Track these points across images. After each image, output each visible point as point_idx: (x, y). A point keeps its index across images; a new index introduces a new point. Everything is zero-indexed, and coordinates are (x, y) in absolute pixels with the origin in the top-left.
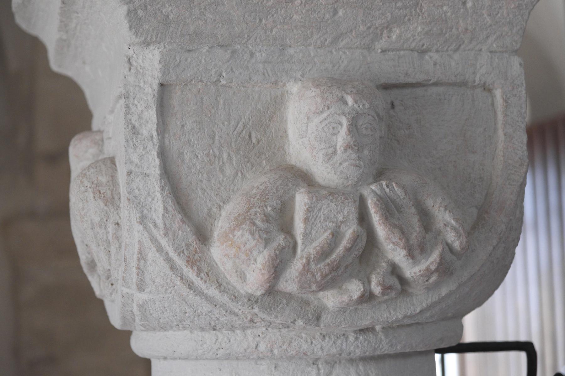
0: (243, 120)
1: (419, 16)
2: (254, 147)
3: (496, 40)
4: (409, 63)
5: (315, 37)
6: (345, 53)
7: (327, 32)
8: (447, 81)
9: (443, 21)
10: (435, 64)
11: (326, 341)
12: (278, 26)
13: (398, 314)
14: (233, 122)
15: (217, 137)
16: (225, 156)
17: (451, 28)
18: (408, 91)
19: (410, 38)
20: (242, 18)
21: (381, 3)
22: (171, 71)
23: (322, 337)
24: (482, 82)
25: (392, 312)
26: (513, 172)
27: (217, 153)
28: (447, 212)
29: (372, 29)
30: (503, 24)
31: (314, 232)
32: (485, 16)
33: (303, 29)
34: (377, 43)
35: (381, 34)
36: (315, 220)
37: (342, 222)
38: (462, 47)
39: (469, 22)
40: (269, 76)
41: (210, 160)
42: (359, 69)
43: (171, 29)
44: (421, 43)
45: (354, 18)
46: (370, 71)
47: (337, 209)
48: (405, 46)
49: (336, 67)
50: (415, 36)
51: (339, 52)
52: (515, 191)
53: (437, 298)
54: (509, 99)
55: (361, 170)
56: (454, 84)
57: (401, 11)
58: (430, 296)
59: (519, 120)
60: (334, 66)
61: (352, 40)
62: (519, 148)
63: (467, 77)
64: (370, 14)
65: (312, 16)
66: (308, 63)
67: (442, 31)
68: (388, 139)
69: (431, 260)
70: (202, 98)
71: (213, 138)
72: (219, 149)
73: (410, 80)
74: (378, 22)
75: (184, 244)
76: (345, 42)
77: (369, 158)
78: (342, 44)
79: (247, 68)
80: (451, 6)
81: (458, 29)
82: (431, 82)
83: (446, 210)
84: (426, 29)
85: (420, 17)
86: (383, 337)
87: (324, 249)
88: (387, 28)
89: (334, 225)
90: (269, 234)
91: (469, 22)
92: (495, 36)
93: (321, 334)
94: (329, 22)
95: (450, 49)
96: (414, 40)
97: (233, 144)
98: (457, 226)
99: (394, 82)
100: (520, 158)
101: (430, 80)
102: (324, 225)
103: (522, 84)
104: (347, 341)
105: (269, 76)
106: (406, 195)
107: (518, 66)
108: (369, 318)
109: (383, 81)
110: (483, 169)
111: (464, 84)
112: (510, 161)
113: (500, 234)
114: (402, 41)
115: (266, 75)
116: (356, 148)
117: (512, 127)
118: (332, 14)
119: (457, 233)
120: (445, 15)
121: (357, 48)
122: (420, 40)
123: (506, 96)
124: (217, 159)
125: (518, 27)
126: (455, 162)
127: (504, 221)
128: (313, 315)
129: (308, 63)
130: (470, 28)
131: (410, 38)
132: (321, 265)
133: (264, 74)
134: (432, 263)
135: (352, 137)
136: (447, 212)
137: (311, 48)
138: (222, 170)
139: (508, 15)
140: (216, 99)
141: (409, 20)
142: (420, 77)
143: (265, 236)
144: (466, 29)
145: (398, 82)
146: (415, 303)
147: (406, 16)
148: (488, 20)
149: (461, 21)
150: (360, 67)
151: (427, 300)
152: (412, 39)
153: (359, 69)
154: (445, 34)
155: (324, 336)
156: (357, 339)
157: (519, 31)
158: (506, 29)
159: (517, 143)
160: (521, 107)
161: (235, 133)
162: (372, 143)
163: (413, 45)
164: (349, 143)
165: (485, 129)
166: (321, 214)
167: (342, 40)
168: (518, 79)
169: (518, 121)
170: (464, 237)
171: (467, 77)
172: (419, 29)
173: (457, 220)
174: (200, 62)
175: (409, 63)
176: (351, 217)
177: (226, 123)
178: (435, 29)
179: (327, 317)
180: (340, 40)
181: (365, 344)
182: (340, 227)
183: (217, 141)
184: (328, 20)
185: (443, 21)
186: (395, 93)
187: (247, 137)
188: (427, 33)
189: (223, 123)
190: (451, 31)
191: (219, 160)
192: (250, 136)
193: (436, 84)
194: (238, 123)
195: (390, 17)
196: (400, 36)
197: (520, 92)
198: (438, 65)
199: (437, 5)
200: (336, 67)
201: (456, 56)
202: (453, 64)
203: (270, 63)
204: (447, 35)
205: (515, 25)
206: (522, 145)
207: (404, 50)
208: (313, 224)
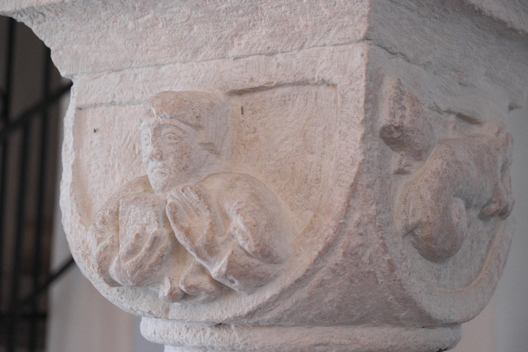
0: (131, 134)
1: (262, 20)
2: (136, 157)
3: (337, 32)
4: (255, 67)
5: (179, 54)
6: (203, 65)
7: (187, 48)
8: (287, 82)
9: (284, 21)
10: (278, 66)
11: (189, 333)
12: (151, 48)
13: (229, 313)
14: (123, 136)
15: (112, 150)
16: (117, 165)
17: (293, 27)
18: (257, 95)
19: (256, 43)
20: (124, 46)
21: (225, 14)
22: (83, 97)
23: (186, 330)
24: (320, 79)
25: (224, 311)
26: (343, 172)
27: (111, 164)
28: (239, 215)
29: (223, 39)
30: (342, 14)
31: (127, 233)
32: (323, 9)
33: (169, 48)
34: (229, 52)
35: (232, 43)
36: (127, 222)
37: (146, 225)
38: (307, 44)
39: (308, 18)
40: (146, 93)
41: (106, 170)
42: (213, 79)
43: (80, 62)
44: (266, 47)
45: (206, 32)
46: (222, 79)
47: (141, 213)
48: (253, 51)
49: (196, 80)
50: (261, 40)
51: (198, 65)
52: (344, 192)
53: (262, 301)
54: (346, 94)
55: (167, 177)
56: (295, 84)
57: (244, 18)
58: (256, 298)
59: (355, 116)
60: (194, 79)
61: (207, 52)
62: (352, 146)
63: (306, 75)
64: (218, 25)
65: (173, 35)
66: (175, 78)
67: (285, 31)
68: (237, 143)
69: (222, 262)
70: (105, 117)
71: (109, 151)
72: (113, 160)
73: (256, 85)
74: (226, 32)
75: (81, 241)
76: (202, 54)
77: (175, 165)
78: (200, 57)
79: (132, 88)
80: (287, 5)
81: (299, 27)
82: (274, 84)
83: (237, 213)
84: (270, 31)
85: (263, 21)
86: (236, 335)
87: (129, 249)
88: (236, 35)
89: (140, 227)
90: (103, 234)
91: (308, 18)
92: (336, 29)
93: (186, 326)
94: (187, 38)
95: (294, 48)
96: (260, 44)
97: (122, 155)
98: (245, 230)
99: (240, 88)
100: (351, 157)
101: (273, 82)
102: (133, 227)
103: (362, 76)
104: (204, 335)
105: (146, 93)
106: (200, 199)
107: (360, 57)
108: (205, 315)
109: (231, 88)
110: (320, 170)
111: (305, 83)
112: (342, 161)
113: (327, 238)
114: (249, 47)
115: (145, 93)
116: (159, 156)
117: (347, 123)
118: (188, 31)
119: (244, 237)
120: (285, 16)
121: (213, 59)
122: (266, 43)
123: (344, 91)
124: (110, 169)
125: (360, 15)
126: (293, 163)
127: (331, 225)
128: (162, 308)
129: (175, 78)
130: (310, 23)
131: (256, 43)
132: (128, 263)
133: (143, 93)
134: (222, 265)
135: (154, 147)
136: (239, 215)
137: (178, 64)
138: (113, 178)
139: (346, 4)
140: (114, 118)
141: (254, 25)
142: (262, 81)
143: (99, 236)
144: (307, 26)
145: (243, 88)
146: (243, 304)
147: (250, 22)
148: (326, 12)
149: (301, 18)
150: (214, 77)
151: (253, 302)
152: (257, 44)
153: (213, 79)
154: (288, 34)
155: (188, 329)
156: (212, 334)
157: (361, 18)
158: (347, 18)
159: (350, 141)
160: (359, 102)
161: (124, 146)
162: (177, 150)
163: (259, 49)
164: (153, 152)
165: (326, 127)
166: (131, 217)
167: (200, 54)
168: (358, 71)
169: (353, 117)
170: (252, 242)
171: (306, 75)
172: (264, 33)
173: (246, 224)
174: (101, 87)
175: (255, 67)
176: (152, 219)
177: (119, 137)
178: (277, 30)
179: (173, 311)
180: (199, 53)
181: (219, 340)
182: (145, 229)
183: (111, 153)
184: (186, 36)
185: (284, 21)
186: (247, 97)
187: (132, 149)
188: (271, 36)
189: (117, 137)
190: (293, 30)
191: (112, 169)
192: (134, 148)
193: (279, 85)
194: (127, 138)
195: (235, 25)
196: (247, 43)
197: (358, 85)
198: (280, 66)
199: (274, 6)
200: (196, 80)
201: (299, 55)
202: (294, 63)
203: (148, 81)
204: (289, 35)
205: (355, 13)
206: (355, 143)
207: (253, 55)
208: (125, 225)
